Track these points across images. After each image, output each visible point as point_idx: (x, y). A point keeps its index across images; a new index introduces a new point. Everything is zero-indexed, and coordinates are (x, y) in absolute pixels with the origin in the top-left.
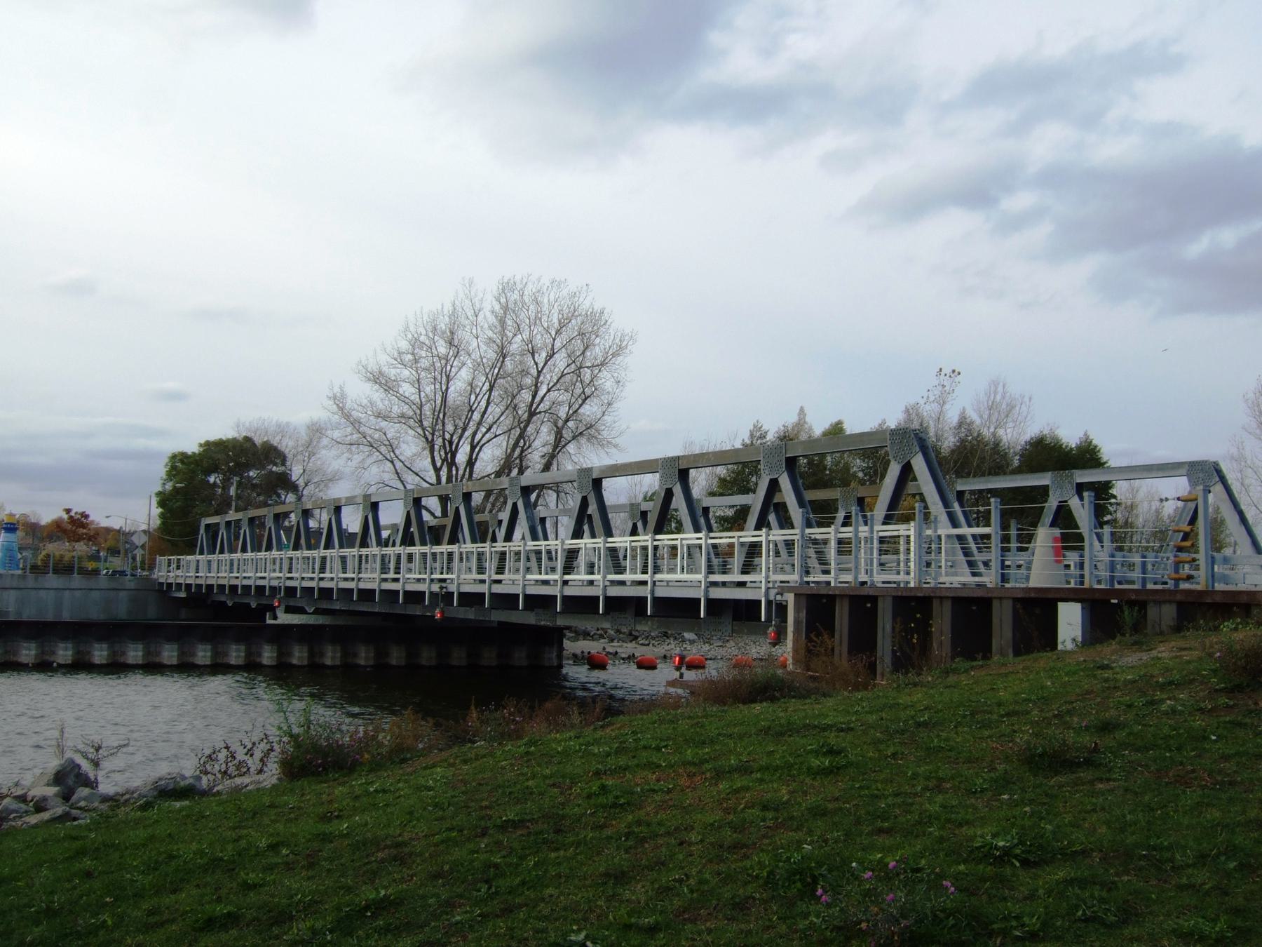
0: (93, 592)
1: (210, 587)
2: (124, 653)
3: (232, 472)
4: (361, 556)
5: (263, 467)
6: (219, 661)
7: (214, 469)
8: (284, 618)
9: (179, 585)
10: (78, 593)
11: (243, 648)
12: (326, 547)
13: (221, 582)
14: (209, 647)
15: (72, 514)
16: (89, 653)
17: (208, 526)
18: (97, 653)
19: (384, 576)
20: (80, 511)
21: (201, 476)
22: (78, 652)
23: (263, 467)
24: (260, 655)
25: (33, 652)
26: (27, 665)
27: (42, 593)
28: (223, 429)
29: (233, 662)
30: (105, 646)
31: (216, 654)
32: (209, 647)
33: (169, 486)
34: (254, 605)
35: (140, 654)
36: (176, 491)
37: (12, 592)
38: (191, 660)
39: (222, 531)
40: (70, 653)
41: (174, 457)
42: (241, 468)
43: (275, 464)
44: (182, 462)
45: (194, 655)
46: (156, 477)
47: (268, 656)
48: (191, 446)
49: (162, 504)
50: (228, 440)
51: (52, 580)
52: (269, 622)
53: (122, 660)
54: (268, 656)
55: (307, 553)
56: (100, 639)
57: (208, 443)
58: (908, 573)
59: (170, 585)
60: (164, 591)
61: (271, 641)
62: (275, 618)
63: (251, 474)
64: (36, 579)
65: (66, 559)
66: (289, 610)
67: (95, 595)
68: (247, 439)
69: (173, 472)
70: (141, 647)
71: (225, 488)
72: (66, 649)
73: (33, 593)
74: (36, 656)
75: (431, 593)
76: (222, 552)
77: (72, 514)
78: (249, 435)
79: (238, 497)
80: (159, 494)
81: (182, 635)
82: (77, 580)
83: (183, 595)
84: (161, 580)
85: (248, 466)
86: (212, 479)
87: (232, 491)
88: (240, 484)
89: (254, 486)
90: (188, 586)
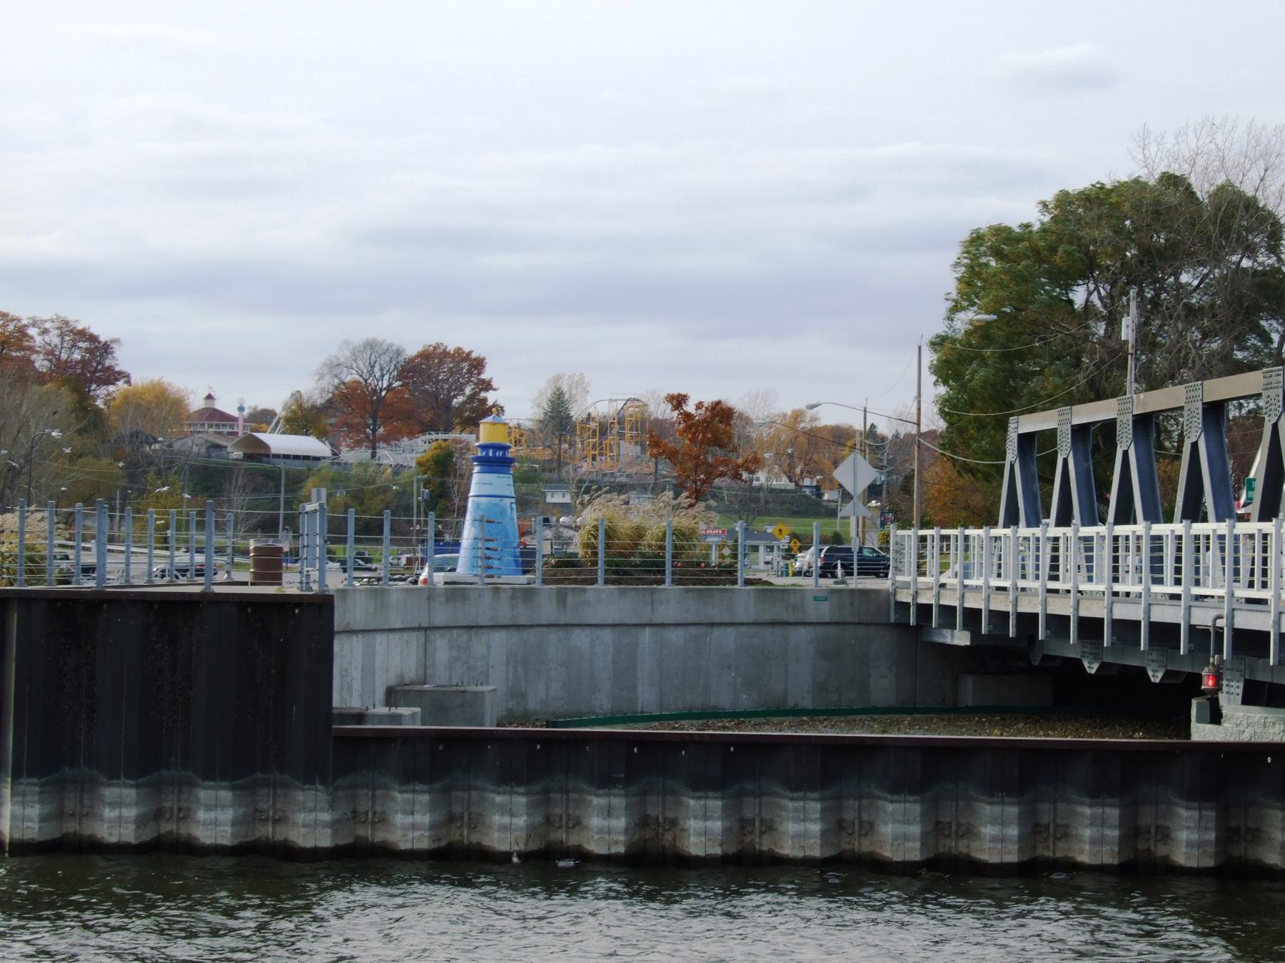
0: (717, 632)
1: (1027, 620)
2: (769, 827)
3: (1131, 275)
4: (1116, 538)
5: (1217, 260)
6: (1046, 851)
7: (1085, 268)
8: (1242, 723)
9: (948, 611)
10: (676, 636)
11: (1113, 813)
12: (1119, 520)
13: (1124, 612)
14: (1013, 811)
15: (690, 408)
16: (674, 823)
17: (1026, 440)
18: (693, 825)
19: (1052, 585)
20: (709, 399)
21: (1049, 290)
22: (644, 822)
23: (1217, 260)
24: (1165, 835)
25: (521, 821)
26: (504, 858)
27: (580, 638)
28: (1109, 157)
29: (1084, 858)
30: (715, 804)
31: (1033, 830)
32: (1013, 811)
33: (966, 319)
34: (1092, 668)
35: (815, 828)
36: (981, 332)
37: (498, 637)
38: (961, 847)
39: (1125, 442)
40: (620, 823)
41: (976, 239)
42: (1152, 264)
43: (1250, 251)
44: (998, 254)
45: (969, 832)
46: (928, 297)
47: (1189, 838)
48: (1023, 210)
49: (945, 371)
50: (1119, 188)
51: (605, 601)
52: (1201, 732)
53: (765, 845)
54: (1189, 838)
55: (1024, 531)
56: (701, 785)
57: (1064, 200)
58: (1264, 585)
59: (925, 610)
60: (911, 625)
61: (1197, 795)
62: (1216, 717)
63: (1184, 278)
64: (561, 598)
65: (648, 539)
66: (1255, 695)
67: (728, 638)
68: (1171, 181)
69: (973, 282)
70: (815, 807)
71: (1113, 321)
72: (609, 812)
73: (553, 636)
74: (531, 831)
75: (1192, 629)
76: (1125, 516)
77: (690, 408)
78: (1176, 170)
79: (1146, 341)
80: (939, 343)
81: (930, 772)
82: (671, 600)
83: (961, 638)
84: (905, 597)
85: (1173, 256)
86: (1079, 296)
87: (1127, 331)
88: (1151, 309)
89: (1192, 313)
90: (972, 617)
